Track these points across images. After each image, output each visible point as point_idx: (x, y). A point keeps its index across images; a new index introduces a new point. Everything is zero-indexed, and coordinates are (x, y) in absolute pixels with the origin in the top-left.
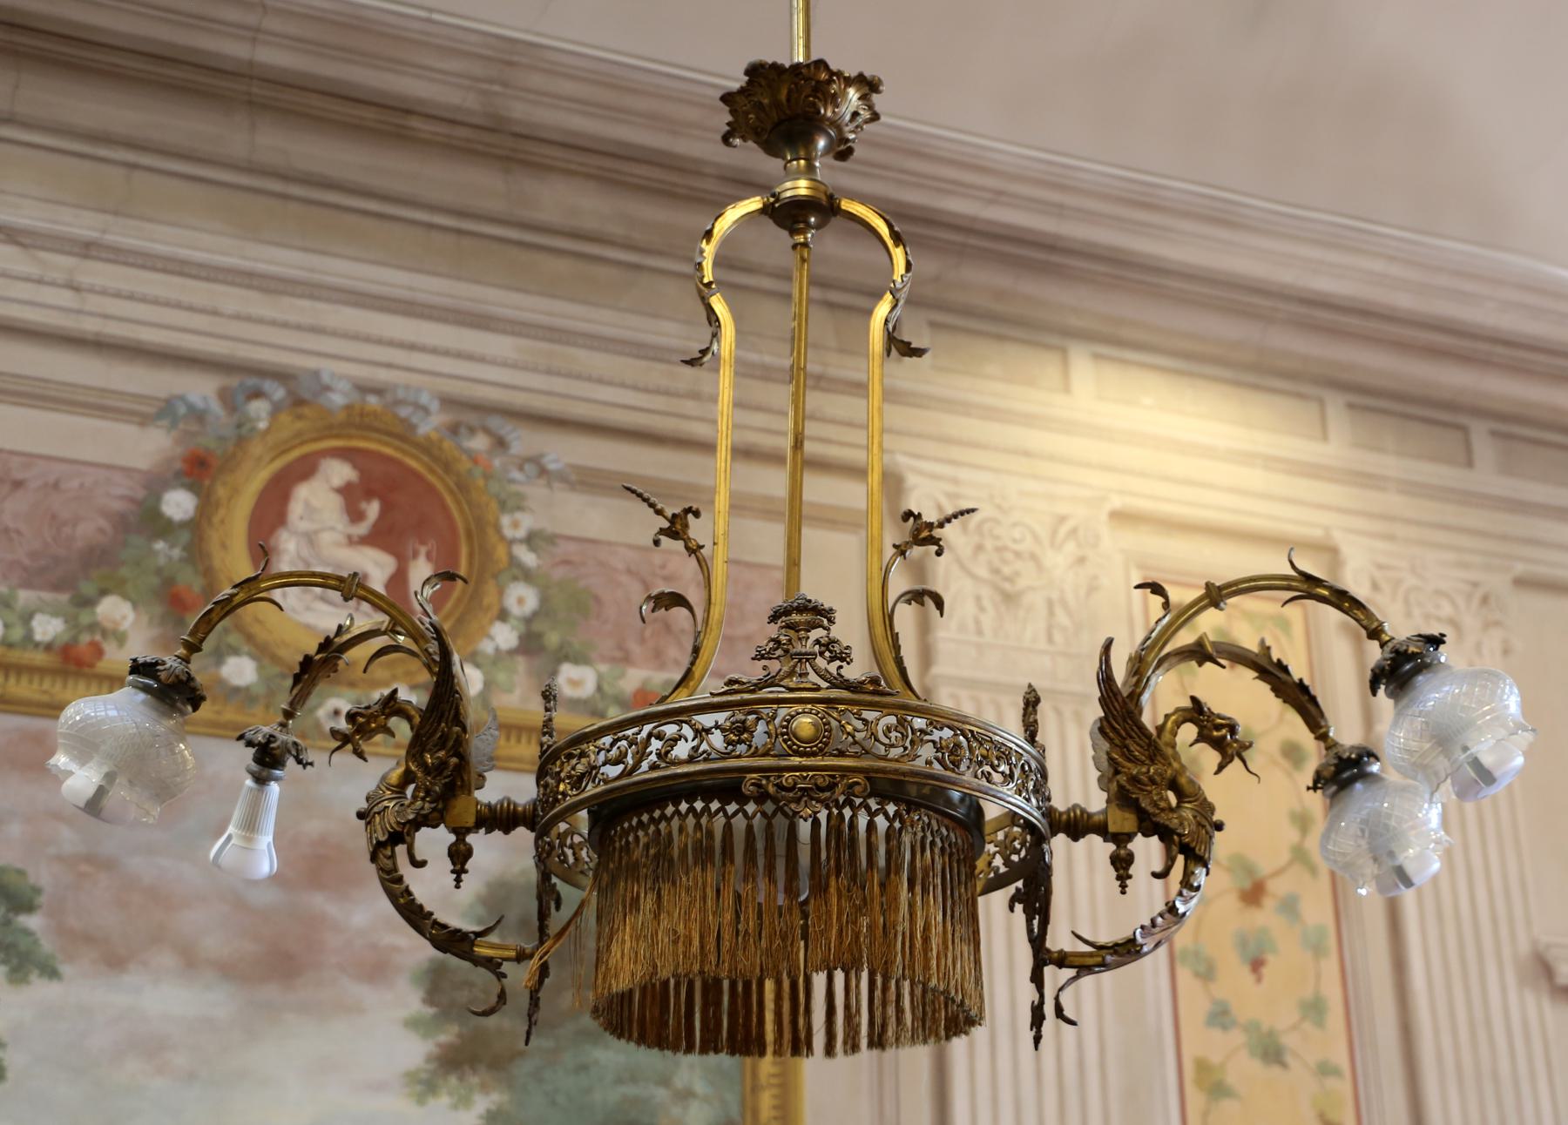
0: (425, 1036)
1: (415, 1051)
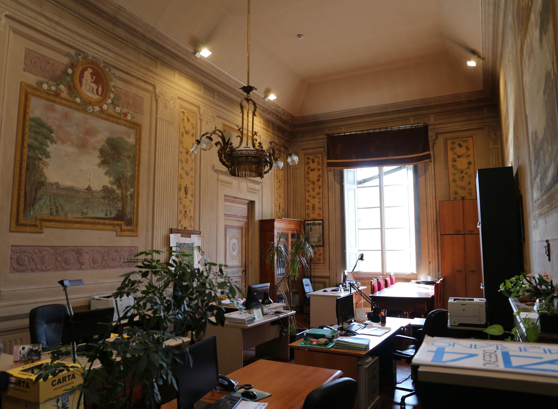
1: (98, 161)
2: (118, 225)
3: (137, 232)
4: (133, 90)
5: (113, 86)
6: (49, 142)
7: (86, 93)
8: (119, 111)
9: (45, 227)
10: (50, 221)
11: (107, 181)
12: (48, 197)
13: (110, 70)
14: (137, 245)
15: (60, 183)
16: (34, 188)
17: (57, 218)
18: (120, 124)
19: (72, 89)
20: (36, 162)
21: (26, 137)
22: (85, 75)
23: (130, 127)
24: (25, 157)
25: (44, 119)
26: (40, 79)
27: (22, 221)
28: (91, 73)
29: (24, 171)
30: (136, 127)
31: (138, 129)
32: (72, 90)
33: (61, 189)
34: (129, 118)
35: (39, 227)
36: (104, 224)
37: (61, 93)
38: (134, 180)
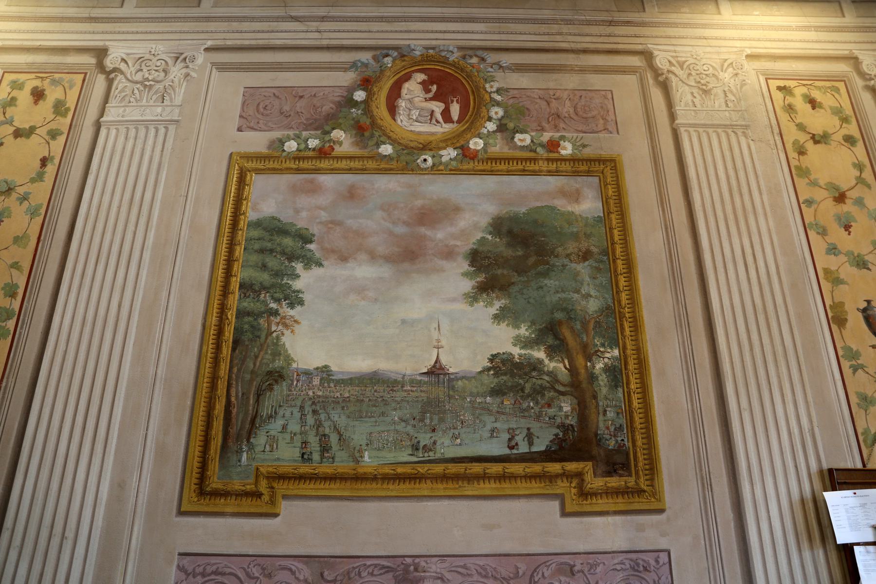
0: (471, 279)
11: (505, 340)
12: (296, 410)
15: (334, 368)
16: (253, 390)
17: (326, 469)
33: (338, 382)
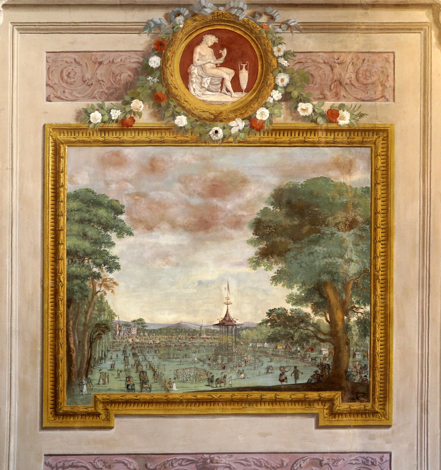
1: (251, 251)
2: (321, 401)
3: (386, 415)
4: (355, 42)
5: (285, 55)
6: (113, 236)
7: (204, 98)
8: (310, 111)
9: (116, 416)
10: (128, 402)
12: (120, 354)
13: (272, 18)
14: (387, 448)
15: (147, 321)
16: (87, 339)
17: (145, 396)
18: (314, 145)
19: (163, 101)
20: (88, 283)
21: (62, 236)
22: (196, 57)
23: (351, 144)
24: (63, 278)
25: (99, 188)
26: (82, 105)
27: (65, 407)
28: (213, 47)
29: (63, 308)
30: (375, 139)
31: (380, 142)
32: (163, 104)
33: (151, 332)
34: (345, 119)
35: (103, 416)
36: (274, 402)
37: (137, 118)
38: (375, 281)
